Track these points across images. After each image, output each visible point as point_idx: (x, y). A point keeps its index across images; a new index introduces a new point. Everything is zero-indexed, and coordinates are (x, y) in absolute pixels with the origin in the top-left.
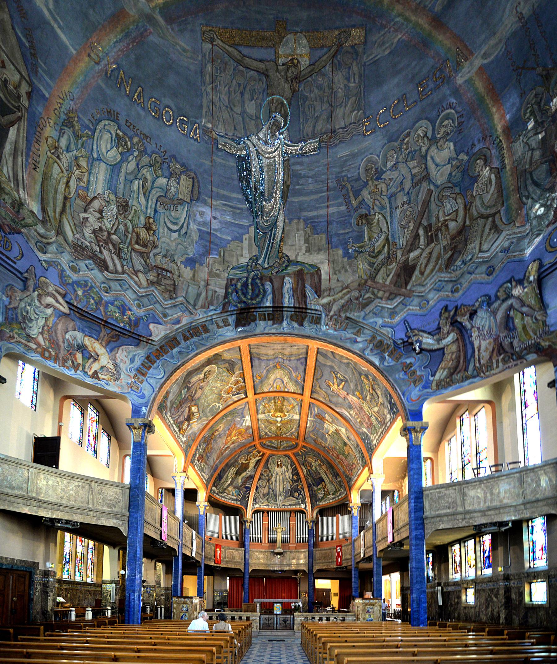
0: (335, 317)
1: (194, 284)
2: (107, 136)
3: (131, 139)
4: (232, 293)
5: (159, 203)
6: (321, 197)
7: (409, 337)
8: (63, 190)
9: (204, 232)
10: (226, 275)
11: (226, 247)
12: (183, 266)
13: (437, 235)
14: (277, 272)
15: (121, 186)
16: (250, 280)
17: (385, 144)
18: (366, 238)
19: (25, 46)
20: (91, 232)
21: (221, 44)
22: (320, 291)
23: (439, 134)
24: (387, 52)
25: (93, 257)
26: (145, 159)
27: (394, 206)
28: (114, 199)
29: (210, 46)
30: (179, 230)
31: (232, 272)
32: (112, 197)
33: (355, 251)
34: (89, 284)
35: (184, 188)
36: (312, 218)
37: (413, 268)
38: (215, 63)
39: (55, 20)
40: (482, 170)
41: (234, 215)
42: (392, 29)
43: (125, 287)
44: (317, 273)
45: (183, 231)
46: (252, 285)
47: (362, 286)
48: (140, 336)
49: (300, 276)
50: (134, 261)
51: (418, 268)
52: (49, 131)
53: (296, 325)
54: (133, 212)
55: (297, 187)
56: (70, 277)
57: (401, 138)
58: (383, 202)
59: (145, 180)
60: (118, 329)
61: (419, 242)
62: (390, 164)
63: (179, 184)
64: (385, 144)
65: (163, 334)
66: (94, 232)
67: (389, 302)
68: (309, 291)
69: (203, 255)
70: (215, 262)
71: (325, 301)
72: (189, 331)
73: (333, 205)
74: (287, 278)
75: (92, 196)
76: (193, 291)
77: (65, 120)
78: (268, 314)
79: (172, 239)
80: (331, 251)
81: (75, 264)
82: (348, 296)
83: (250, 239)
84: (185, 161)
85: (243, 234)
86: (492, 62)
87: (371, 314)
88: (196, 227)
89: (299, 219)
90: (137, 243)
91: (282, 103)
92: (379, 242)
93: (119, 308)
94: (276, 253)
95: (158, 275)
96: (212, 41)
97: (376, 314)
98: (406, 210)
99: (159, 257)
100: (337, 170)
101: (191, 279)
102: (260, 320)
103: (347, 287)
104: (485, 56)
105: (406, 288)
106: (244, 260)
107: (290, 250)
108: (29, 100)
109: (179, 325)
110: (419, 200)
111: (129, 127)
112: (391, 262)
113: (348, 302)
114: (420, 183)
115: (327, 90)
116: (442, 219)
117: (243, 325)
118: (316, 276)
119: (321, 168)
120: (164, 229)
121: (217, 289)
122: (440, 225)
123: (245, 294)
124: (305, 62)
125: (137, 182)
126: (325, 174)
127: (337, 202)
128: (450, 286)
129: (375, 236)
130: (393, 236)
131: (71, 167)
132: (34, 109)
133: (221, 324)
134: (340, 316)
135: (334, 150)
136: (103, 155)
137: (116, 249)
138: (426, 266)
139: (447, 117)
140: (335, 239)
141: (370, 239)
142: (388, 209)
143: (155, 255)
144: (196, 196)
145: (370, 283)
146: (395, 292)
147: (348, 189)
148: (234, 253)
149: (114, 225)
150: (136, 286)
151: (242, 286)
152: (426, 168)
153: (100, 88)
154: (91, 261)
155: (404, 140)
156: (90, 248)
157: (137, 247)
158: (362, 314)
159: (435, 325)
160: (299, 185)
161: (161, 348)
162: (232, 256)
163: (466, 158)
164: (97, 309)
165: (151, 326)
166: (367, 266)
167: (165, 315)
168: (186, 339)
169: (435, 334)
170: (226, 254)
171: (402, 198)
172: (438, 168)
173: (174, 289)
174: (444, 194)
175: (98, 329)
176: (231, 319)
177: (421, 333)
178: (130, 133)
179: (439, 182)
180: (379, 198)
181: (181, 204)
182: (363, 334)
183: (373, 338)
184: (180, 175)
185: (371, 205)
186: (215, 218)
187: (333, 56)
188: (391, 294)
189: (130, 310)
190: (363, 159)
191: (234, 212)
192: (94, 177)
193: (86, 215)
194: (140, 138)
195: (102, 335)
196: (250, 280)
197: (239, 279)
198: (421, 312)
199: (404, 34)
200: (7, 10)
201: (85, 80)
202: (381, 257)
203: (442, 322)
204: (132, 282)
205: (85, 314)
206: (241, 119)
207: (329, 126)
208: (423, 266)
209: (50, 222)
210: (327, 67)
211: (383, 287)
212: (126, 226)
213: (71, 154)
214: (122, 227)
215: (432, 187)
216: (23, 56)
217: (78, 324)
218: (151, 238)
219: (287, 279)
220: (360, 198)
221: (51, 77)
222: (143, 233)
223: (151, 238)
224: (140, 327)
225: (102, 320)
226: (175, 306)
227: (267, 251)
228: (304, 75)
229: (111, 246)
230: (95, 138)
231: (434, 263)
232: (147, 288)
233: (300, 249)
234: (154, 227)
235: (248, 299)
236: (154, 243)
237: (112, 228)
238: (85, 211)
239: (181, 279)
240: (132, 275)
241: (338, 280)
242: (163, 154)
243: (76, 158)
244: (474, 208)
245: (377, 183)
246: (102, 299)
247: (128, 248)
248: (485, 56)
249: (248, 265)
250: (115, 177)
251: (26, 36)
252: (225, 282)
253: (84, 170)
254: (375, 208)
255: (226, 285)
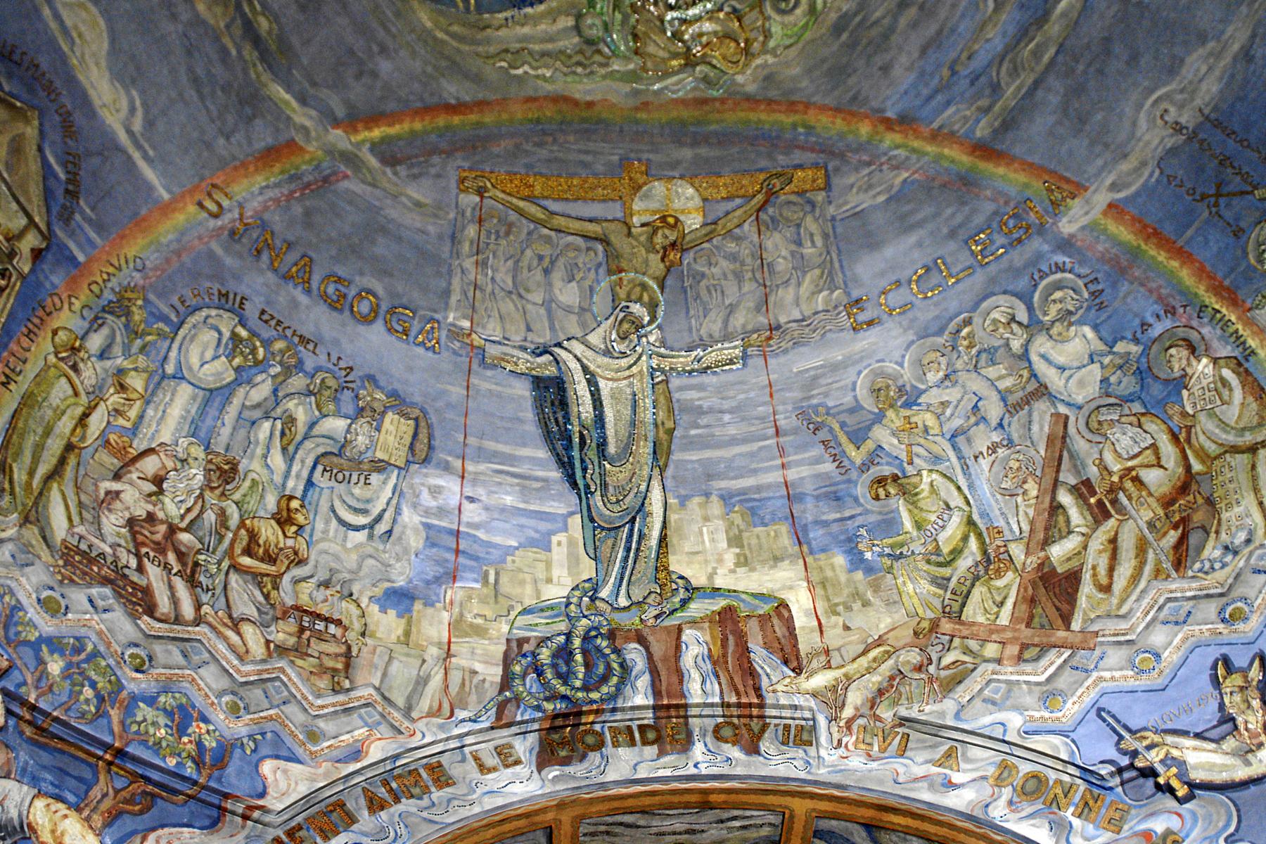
0: (861, 721)
1: (408, 655)
2: (209, 336)
3: (267, 344)
4: (524, 677)
5: (320, 468)
6: (761, 448)
7: (1134, 754)
8: (67, 431)
9: (440, 530)
10: (505, 628)
11: (504, 561)
12: (375, 608)
13: (1114, 502)
14: (656, 617)
15: (226, 432)
16: (577, 642)
17: (913, 342)
18: (908, 525)
19: (56, 177)
20: (122, 522)
21: (501, 195)
22: (798, 657)
23: (1045, 314)
24: (881, 199)
25: (117, 580)
26: (298, 382)
27: (968, 452)
28: (202, 455)
29: (478, 199)
30: (371, 526)
31: (522, 621)
32: (198, 451)
33: (881, 555)
34: (90, 647)
35: (391, 439)
36: (742, 492)
37: (1074, 578)
38: (487, 225)
39: (139, 147)
40: (1189, 364)
41: (525, 492)
42: (885, 167)
43: (196, 659)
44: (780, 615)
45: (382, 528)
46: (585, 652)
47: (925, 634)
48: (226, 796)
49: (727, 620)
50: (233, 596)
51: (1087, 577)
52: (68, 320)
53: (736, 753)
54: (247, 483)
55: (693, 432)
56: (36, 627)
57: (952, 327)
58: (935, 449)
59: (290, 420)
60: (155, 776)
61: (1068, 521)
62: (932, 377)
63: (378, 429)
64: (913, 342)
65: (303, 789)
66: (131, 522)
67: (1028, 667)
68: (760, 657)
69: (437, 580)
70: (470, 598)
71: (820, 680)
72: (385, 783)
73: (799, 463)
74: (688, 632)
75: (143, 447)
76: (402, 672)
77: (110, 302)
78: (641, 727)
79: (349, 545)
80: (809, 560)
81: (56, 595)
82: (891, 662)
83: (571, 543)
84: (397, 386)
85: (554, 533)
86: (1138, 194)
87: (978, 703)
88: (417, 519)
89: (707, 495)
90: (248, 552)
91: (644, 287)
92: (949, 532)
93: (169, 714)
94: (651, 571)
95: (302, 630)
96: (481, 192)
97: (994, 703)
98: (1007, 459)
99: (307, 588)
100: (797, 394)
101: (399, 642)
102: (616, 744)
103: (879, 642)
104: (1114, 187)
105: (1068, 628)
106: (556, 592)
107: (689, 563)
108: (34, 263)
109: (359, 765)
110: (1035, 437)
111: (266, 322)
112: (998, 571)
113: (892, 678)
114: (1028, 403)
115: (749, 260)
116: (1116, 467)
117: (566, 762)
118: (776, 621)
119: (752, 394)
120: (327, 522)
121: (478, 667)
122: (1115, 479)
123: (565, 678)
124: (693, 222)
125: (267, 425)
126: (764, 404)
127: (806, 455)
128: (1211, 608)
129: (933, 518)
130: (984, 515)
131: (101, 388)
132: (42, 277)
133: (491, 761)
134: (877, 718)
135: (782, 359)
136: (190, 369)
137: (184, 564)
138: (1111, 570)
139: (1058, 286)
140: (816, 534)
141: (918, 526)
142: (954, 459)
143: (296, 582)
144: (422, 451)
145: (946, 626)
146: (1036, 640)
147: (831, 430)
148: (528, 577)
149: (189, 510)
150: (232, 657)
151: (555, 656)
152: (1034, 375)
153: (211, 255)
154: (107, 591)
155: (958, 331)
156: (110, 559)
157: (246, 561)
158: (949, 705)
159: (1209, 714)
160: (698, 427)
161: (291, 833)
162: (522, 583)
163: (1135, 349)
164: (100, 714)
165: (267, 767)
166: (926, 587)
167: (313, 736)
168: (376, 805)
169: (1223, 738)
170: (504, 579)
171: (983, 439)
172: (1067, 373)
173: (347, 666)
174: (1102, 418)
175: (87, 774)
176: (524, 747)
177: (1170, 739)
178: (267, 333)
179: (1079, 399)
180: (922, 441)
181: (379, 470)
182: (968, 760)
183: (1005, 768)
184: (383, 414)
185: (903, 456)
186: (471, 500)
187: (758, 211)
188: (1024, 647)
189: (206, 720)
190: (859, 373)
191: (524, 487)
192: (156, 410)
193: (115, 486)
194: (290, 342)
195: (96, 793)
196: (577, 642)
197: (542, 641)
198: (1144, 682)
199: (914, 173)
200: (36, 123)
201: (179, 241)
202: (964, 564)
203: (1233, 703)
204: (222, 647)
205: (55, 729)
206: (542, 311)
207: (763, 320)
208: (1102, 571)
209: (12, 493)
210: (746, 226)
211: (992, 632)
212: (223, 515)
213: (108, 363)
214: (210, 517)
215: (1063, 409)
216: (48, 195)
217: (23, 757)
218: (290, 542)
219: (688, 634)
220: (869, 445)
221: (100, 227)
222: (269, 532)
223: (290, 542)
224: (231, 770)
225: (107, 747)
226: (347, 711)
227: (624, 568)
228: (693, 240)
229: (171, 557)
230: (179, 338)
231: (1133, 562)
232: (263, 661)
233: (720, 561)
234: (300, 518)
235: (573, 688)
236: (296, 553)
237: (183, 517)
238: (117, 477)
239: (368, 640)
240: (222, 629)
241: (847, 628)
242: (344, 373)
243: (121, 372)
244: (1202, 438)
245: (907, 413)
246: (121, 688)
247: (219, 563)
248: (1114, 187)
249: (568, 605)
250: (213, 412)
251: (64, 165)
252: (504, 648)
253: (134, 396)
254: (916, 460)
255: (506, 655)
